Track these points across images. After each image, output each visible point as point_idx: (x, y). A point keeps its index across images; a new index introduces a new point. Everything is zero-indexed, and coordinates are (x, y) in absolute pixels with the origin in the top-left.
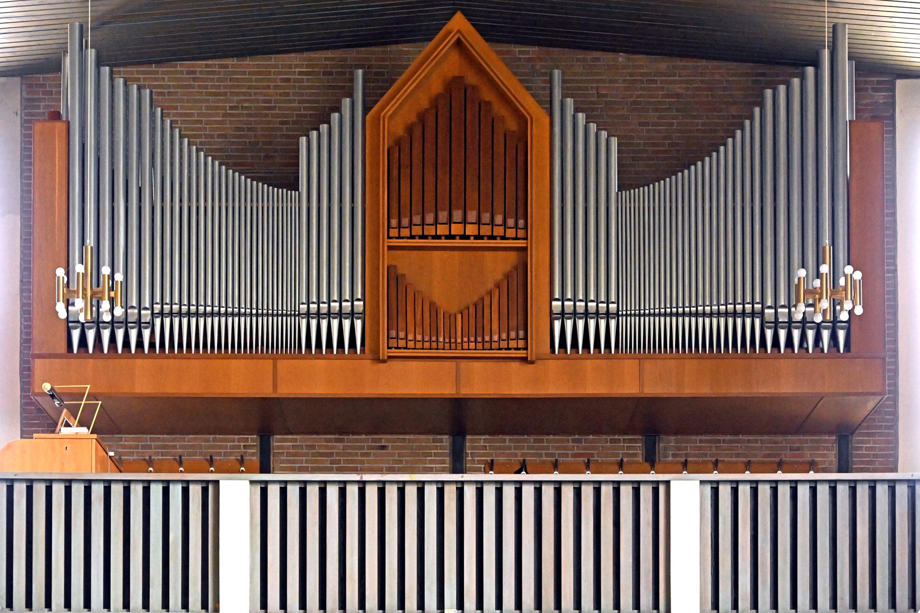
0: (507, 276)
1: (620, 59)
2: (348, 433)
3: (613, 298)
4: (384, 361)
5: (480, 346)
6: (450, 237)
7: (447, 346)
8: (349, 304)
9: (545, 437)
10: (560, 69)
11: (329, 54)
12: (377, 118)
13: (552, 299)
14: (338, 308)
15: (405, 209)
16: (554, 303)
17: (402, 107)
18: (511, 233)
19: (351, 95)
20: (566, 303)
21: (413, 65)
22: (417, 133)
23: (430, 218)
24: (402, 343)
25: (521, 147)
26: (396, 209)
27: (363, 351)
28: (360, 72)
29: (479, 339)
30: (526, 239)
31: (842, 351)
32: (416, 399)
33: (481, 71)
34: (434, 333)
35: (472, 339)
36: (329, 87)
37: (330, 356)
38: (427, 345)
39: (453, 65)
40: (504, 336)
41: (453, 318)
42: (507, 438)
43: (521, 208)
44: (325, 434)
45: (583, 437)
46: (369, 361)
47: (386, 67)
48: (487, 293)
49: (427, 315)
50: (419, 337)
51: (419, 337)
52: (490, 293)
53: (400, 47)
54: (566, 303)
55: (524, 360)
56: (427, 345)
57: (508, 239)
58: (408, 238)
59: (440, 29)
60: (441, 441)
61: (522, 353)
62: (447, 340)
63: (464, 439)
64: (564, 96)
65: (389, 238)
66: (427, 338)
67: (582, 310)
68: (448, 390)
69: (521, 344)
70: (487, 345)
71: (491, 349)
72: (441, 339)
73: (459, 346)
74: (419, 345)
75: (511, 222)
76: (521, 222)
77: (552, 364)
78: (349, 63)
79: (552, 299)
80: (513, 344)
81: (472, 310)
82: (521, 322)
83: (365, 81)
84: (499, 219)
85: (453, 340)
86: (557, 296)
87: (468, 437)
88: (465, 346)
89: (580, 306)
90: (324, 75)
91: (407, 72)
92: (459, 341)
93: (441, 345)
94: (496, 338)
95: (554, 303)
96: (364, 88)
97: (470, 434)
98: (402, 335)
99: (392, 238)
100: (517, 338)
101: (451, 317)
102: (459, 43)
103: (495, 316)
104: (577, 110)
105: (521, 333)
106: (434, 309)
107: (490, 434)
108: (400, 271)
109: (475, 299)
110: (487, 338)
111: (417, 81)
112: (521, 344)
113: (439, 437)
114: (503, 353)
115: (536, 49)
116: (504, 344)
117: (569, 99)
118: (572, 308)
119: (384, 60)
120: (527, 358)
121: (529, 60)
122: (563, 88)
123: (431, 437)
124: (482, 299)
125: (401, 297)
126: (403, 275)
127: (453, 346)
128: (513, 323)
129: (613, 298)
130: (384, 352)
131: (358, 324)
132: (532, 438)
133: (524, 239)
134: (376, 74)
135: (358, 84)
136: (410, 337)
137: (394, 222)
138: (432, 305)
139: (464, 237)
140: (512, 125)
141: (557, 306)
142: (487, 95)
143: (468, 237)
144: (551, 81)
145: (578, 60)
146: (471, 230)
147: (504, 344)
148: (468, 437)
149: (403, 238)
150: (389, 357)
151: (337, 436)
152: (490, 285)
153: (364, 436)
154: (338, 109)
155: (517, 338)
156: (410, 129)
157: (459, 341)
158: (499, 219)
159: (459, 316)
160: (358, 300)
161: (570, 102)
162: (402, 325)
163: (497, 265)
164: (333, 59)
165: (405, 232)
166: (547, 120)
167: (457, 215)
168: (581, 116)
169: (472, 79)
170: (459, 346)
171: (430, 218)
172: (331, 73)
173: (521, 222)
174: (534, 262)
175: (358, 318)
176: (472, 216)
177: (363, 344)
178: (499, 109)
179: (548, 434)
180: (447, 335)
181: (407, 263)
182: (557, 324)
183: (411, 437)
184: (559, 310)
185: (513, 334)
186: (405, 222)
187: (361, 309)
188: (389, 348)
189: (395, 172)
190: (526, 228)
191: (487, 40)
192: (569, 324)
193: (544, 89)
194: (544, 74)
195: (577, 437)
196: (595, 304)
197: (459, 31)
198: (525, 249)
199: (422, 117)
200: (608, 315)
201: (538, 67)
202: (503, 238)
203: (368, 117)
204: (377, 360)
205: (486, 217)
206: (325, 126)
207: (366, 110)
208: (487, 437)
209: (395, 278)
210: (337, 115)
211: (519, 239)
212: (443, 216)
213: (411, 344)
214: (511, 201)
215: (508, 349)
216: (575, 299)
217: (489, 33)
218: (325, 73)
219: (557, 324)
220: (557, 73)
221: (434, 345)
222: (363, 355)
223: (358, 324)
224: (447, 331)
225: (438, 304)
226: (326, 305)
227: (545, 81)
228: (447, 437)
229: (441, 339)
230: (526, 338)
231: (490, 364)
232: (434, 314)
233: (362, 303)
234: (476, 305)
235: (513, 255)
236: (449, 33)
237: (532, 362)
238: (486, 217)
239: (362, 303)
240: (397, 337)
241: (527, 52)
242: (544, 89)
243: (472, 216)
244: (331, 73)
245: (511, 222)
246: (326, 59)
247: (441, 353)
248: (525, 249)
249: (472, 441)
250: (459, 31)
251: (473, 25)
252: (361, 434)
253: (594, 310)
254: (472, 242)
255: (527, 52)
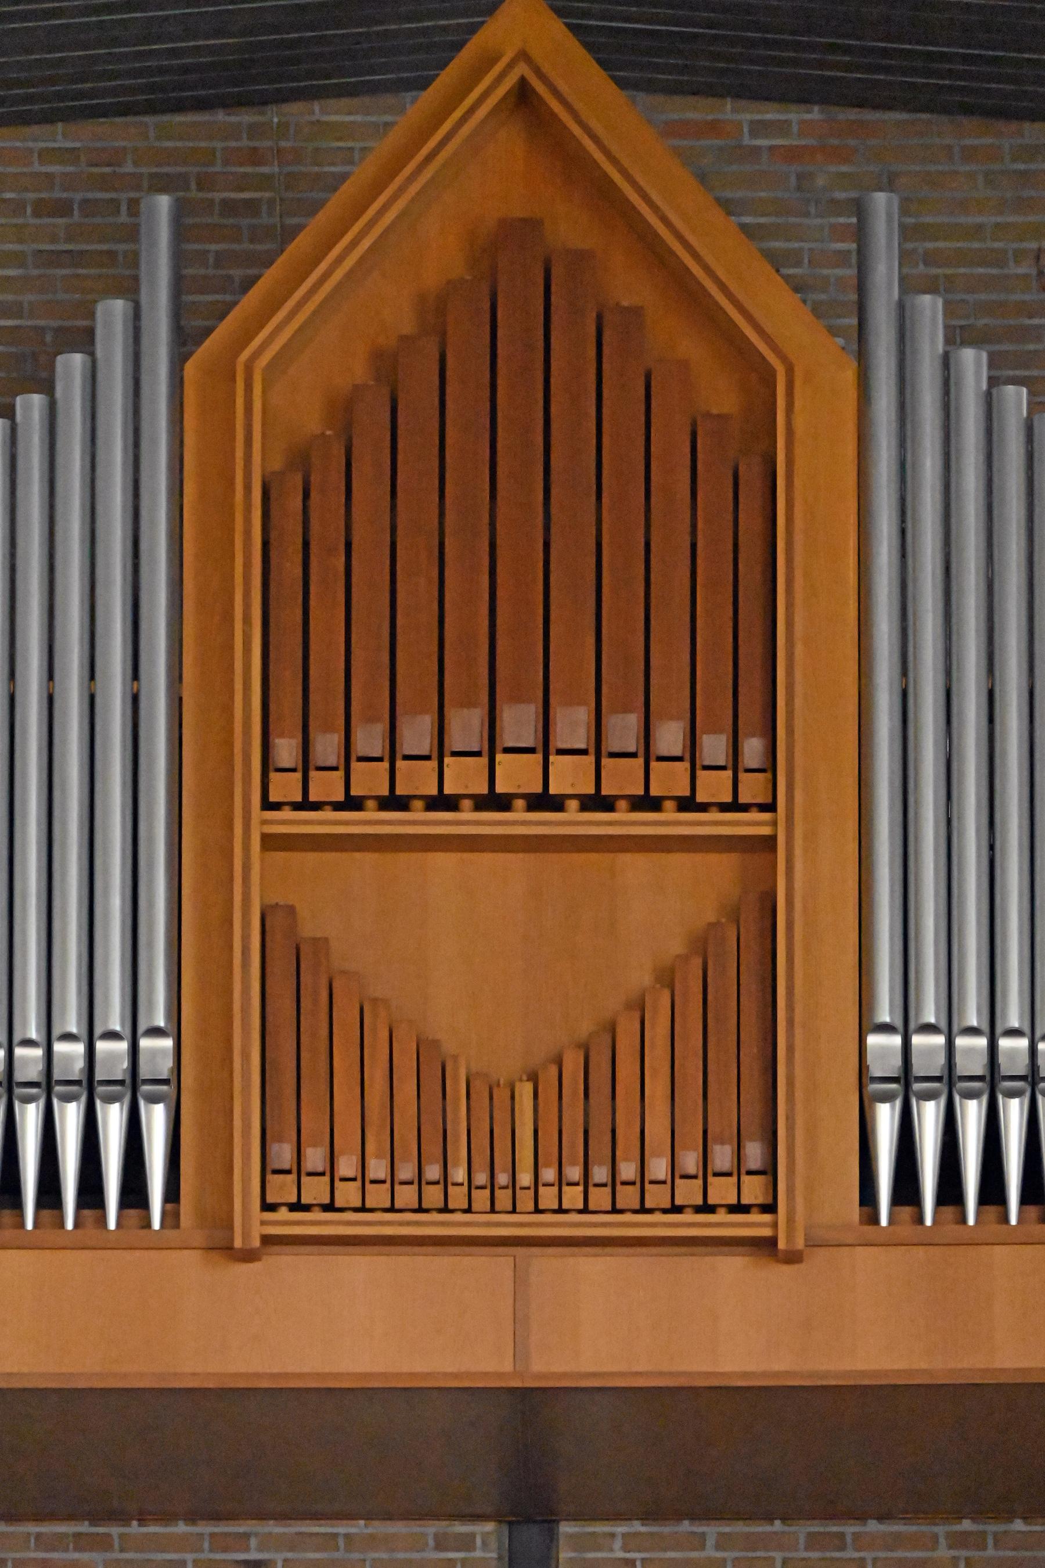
0: (702, 945)
1: (821, 183)
2: (120, 1517)
3: (1013, 1016)
4: (249, 1256)
5: (600, 1198)
6: (494, 801)
7: (481, 1198)
8: (123, 1046)
9: (850, 1529)
10: (897, 190)
11: (60, 136)
12: (224, 373)
13: (866, 1024)
14: (80, 1064)
15: (327, 701)
16: (873, 1040)
17: (317, 329)
18: (714, 787)
19: (129, 288)
20: (918, 1040)
21: (363, 173)
22: (373, 420)
23: (416, 735)
24: (315, 1191)
25: (751, 473)
26: (293, 695)
27: (171, 1218)
28: (164, 202)
29: (600, 1173)
30: (770, 807)
31: (156, 1224)
32: (694, 1391)
33: (605, 199)
34: (432, 1148)
35: (574, 1173)
36: (54, 259)
37: (50, 1235)
38: (406, 1196)
39: (497, 179)
40: (690, 1162)
41: (501, 1096)
42: (711, 1530)
43: (752, 694)
44: (39, 1517)
45: (992, 1528)
46: (192, 1257)
47: (265, 182)
48: (629, 1006)
49: (406, 1090)
50: (377, 1168)
51: (377, 1168)
52: (639, 1006)
53: (319, 111)
54: (918, 1040)
55: (766, 1246)
56: (406, 1196)
57: (704, 808)
58: (338, 807)
59: (458, 46)
60: (466, 1543)
61: (756, 1225)
62: (481, 1178)
63: (551, 1536)
64: (909, 286)
65: (268, 805)
66: (406, 1171)
67: (977, 1066)
68: (479, 1355)
69: (753, 1190)
70: (628, 1197)
71: (643, 1210)
72: (459, 1174)
73: (526, 1201)
74: (378, 1196)
75: (714, 747)
76: (753, 749)
77: (866, 1258)
78: (128, 168)
79: (866, 1024)
80: (722, 1191)
81: (573, 1063)
82: (753, 1108)
83: (180, 233)
84: (670, 737)
85: (502, 1179)
86: (885, 1017)
87: (566, 1528)
88: (548, 1197)
89: (970, 1051)
90: (36, 214)
91: (335, 205)
92: (525, 1178)
93: (458, 1197)
94: (659, 1168)
95: (873, 1040)
96: (179, 259)
97: (575, 1517)
98: (315, 1157)
99: (277, 806)
100: (738, 1170)
101: (492, 1094)
102: (523, 95)
103: (657, 1088)
104: (958, 336)
105: (754, 1153)
106: (433, 1065)
107: (646, 1517)
108: (308, 929)
109: (585, 1028)
110: (628, 1170)
111: (366, 243)
112: (753, 1190)
113: (461, 1528)
114: (690, 1225)
115: (815, 114)
116: (689, 1192)
117: (927, 299)
118: (941, 1059)
119: (255, 157)
120: (773, 1241)
121: (792, 154)
122: (905, 256)
123: (431, 1529)
124: (612, 1029)
125: (314, 1023)
126: (321, 944)
127: (503, 1198)
128: (723, 1120)
129: (1013, 1016)
130: (250, 1224)
131: (156, 1121)
132: (801, 1530)
133: (764, 808)
134: (229, 208)
135: (153, 244)
136: (347, 1166)
137: (286, 751)
138: (425, 1047)
139: (544, 801)
140: (721, 396)
141: (884, 1050)
142: (629, 286)
143: (556, 804)
144: (861, 234)
145: (969, 154)
146: (569, 776)
147: (689, 1192)
148: (566, 1528)
149: (317, 806)
150: (268, 1240)
151: (84, 1527)
152: (640, 976)
153: (182, 1528)
154: (84, 340)
155: (738, 1170)
156: (343, 412)
157: (525, 1178)
158: (670, 737)
159: (525, 1090)
160: (156, 1032)
161: (930, 308)
162: (313, 1122)
163: (662, 902)
164: (70, 155)
165: (327, 786)
166: (850, 375)
167: (519, 723)
168: (972, 363)
169: (570, 227)
170: (526, 1201)
171: (416, 735)
172: (62, 209)
173: (753, 749)
174: (798, 884)
175: (153, 1099)
176: (572, 725)
177: (172, 1193)
178: (674, 339)
179: (862, 1517)
180: (481, 1160)
181: (344, 903)
182: (886, 1120)
183: (356, 1528)
184: (893, 1065)
185: (722, 1156)
186: (327, 747)
187: (165, 1067)
188: (268, 1207)
189: (289, 568)
190: (770, 766)
191: (622, 84)
192: (929, 1117)
193: (842, 258)
194: (835, 207)
195: (967, 1525)
196: (1023, 1043)
197: (524, 56)
198: (769, 843)
199: (387, 365)
200: (992, 1082)
201: (820, 181)
202: (687, 804)
203: (190, 368)
204: (225, 1249)
205: (624, 731)
206: (37, 400)
207: (185, 341)
208: (637, 1527)
209: (291, 957)
210: (77, 360)
211: (745, 808)
212: (466, 727)
213: (348, 1194)
214: (714, 672)
215: (707, 1208)
216: (950, 1027)
217: (628, 59)
218: (41, 209)
219: (886, 1120)
220: (882, 204)
221: (433, 1196)
222: (171, 1233)
223: (156, 1121)
224: (481, 1141)
225: (449, 1046)
226: (38, 1052)
227: (838, 233)
228: (490, 1527)
229: (459, 1174)
230: (770, 1170)
231: (442, 1262)
232: (432, 1086)
233: (168, 1043)
234: (586, 1049)
235: (723, 866)
236: (489, 61)
237: (793, 1258)
238: (624, 731)
239: (168, 1043)
240: (298, 1169)
241: (782, 128)
242: (842, 258)
243: (572, 725)
244: (62, 209)
245: (714, 747)
246: (45, 155)
247: (457, 1225)
248: (769, 843)
249: (579, 1543)
250: (524, 56)
251: (573, 28)
252: (168, 1517)
253: (937, 1065)
254: (573, 821)
255: (782, 128)
